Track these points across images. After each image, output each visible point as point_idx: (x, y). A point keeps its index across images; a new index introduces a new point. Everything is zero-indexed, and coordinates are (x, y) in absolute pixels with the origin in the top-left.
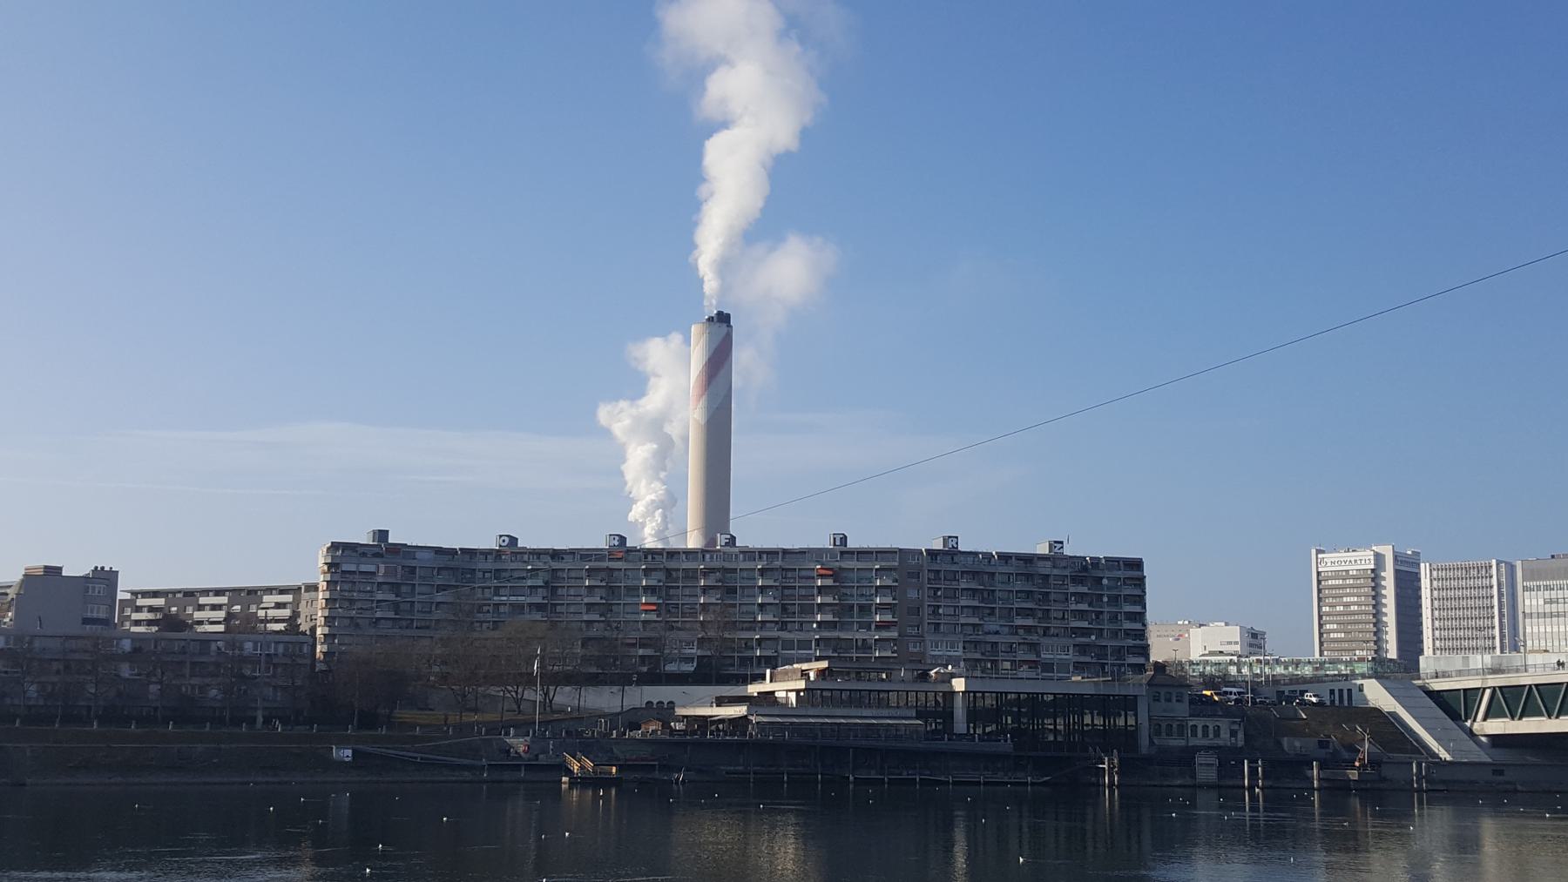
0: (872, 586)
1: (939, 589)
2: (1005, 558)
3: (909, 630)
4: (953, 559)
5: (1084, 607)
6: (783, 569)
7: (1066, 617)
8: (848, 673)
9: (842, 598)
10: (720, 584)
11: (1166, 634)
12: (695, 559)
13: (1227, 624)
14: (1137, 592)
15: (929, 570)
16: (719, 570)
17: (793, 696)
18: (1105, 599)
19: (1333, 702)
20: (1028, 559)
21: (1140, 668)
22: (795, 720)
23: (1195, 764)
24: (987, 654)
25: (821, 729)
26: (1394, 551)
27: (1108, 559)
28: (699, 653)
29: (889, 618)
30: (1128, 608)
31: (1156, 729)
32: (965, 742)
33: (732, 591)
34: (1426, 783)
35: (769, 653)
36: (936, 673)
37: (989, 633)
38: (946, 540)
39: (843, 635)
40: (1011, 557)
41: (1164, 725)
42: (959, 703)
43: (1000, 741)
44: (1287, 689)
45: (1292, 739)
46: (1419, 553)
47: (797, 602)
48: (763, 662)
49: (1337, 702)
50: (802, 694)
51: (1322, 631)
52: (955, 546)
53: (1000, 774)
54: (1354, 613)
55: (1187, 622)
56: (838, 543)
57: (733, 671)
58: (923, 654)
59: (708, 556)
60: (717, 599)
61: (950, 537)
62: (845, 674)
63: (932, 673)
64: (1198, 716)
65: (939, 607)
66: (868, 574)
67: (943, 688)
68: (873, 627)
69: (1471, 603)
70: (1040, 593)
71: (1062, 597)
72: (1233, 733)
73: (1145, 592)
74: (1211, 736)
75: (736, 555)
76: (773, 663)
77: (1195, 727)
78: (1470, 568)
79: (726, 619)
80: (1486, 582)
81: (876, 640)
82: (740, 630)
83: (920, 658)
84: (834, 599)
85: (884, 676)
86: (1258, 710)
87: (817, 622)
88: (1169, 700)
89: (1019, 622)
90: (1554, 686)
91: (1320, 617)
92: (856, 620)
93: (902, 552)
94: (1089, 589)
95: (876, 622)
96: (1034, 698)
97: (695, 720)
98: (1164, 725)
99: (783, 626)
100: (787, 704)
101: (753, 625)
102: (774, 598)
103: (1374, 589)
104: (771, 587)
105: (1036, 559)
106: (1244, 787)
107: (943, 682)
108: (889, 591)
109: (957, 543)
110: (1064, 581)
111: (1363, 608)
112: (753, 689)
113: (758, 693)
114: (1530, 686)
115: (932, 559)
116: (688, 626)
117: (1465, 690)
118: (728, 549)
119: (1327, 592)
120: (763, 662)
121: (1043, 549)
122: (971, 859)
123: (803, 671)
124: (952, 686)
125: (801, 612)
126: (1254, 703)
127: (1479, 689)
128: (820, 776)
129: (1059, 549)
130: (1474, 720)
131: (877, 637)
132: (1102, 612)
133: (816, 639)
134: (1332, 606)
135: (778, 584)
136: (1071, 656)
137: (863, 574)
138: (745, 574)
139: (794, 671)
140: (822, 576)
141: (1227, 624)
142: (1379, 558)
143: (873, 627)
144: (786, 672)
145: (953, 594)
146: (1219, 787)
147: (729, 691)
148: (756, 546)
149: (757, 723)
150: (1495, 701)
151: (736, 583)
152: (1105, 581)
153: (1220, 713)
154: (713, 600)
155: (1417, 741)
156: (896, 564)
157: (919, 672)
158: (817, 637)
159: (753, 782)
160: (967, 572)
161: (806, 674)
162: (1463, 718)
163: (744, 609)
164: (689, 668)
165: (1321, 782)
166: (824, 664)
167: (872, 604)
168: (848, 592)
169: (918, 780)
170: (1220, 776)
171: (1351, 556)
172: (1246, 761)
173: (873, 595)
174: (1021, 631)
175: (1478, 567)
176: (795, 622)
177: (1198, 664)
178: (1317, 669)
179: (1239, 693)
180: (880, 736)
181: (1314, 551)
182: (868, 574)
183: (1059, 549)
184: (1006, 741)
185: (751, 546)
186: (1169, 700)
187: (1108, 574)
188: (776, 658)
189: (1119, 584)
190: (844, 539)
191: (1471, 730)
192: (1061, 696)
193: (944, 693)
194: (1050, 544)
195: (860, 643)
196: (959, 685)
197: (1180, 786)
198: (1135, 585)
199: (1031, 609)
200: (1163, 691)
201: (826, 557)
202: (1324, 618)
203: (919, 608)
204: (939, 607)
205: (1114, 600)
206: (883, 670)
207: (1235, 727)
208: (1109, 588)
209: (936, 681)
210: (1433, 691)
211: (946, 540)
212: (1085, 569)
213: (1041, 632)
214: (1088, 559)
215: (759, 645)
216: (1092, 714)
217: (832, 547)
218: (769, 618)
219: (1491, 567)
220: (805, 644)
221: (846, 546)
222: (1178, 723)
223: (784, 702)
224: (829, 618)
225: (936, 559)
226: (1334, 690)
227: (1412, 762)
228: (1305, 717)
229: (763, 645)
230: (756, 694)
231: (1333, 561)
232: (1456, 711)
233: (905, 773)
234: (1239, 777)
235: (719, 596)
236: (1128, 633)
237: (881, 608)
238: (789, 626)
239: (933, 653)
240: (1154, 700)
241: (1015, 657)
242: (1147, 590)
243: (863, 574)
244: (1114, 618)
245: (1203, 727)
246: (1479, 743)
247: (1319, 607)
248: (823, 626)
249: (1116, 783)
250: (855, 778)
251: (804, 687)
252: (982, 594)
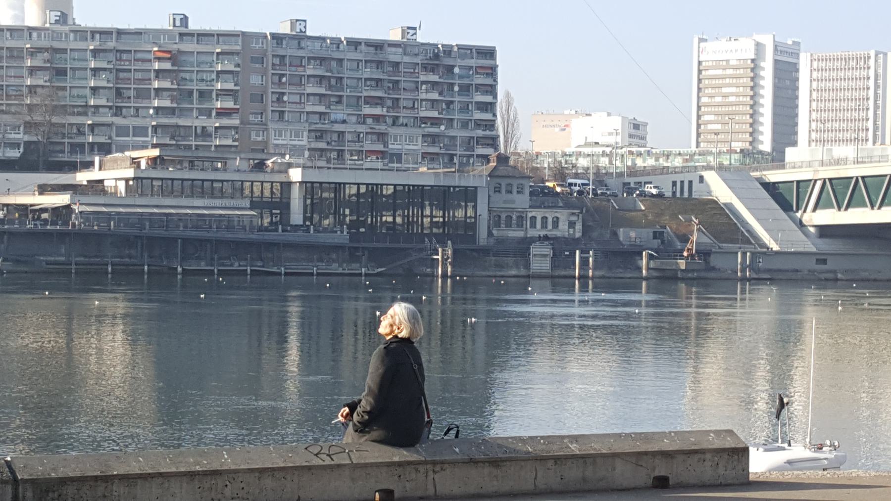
0: (213, 71)
1: (283, 75)
2: (354, 44)
3: (252, 118)
4: (299, 43)
5: (435, 96)
6: (117, 51)
7: (416, 107)
8: (181, 162)
9: (181, 83)
10: (49, 65)
11: (552, 124)
12: (21, 37)
13: (609, 114)
14: (489, 81)
15: (273, 55)
16: (47, 50)
17: (122, 186)
18: (456, 88)
19: (674, 193)
20: (378, 46)
21: (486, 158)
22: (121, 210)
23: (529, 254)
24: (333, 143)
25: (150, 220)
26: (774, 41)
27: (460, 47)
28: (26, 138)
29: (230, 104)
30: (479, 98)
31: (496, 220)
32: (300, 233)
33: (61, 73)
34: (750, 271)
35: (102, 139)
36: (272, 163)
37: (336, 122)
38: (294, 23)
39: (182, 122)
40: (360, 43)
41: (503, 216)
42: (296, 194)
43: (336, 232)
44: (632, 180)
45: (627, 229)
46: (800, 43)
47: (133, 86)
48: (96, 149)
49: (678, 195)
50: (131, 183)
51: (700, 122)
52: (303, 30)
53: (335, 265)
54: (731, 104)
55: (573, 112)
56: (178, 23)
57: (65, 157)
58: (266, 143)
59: (35, 35)
60: (46, 81)
61: (297, 20)
62: (178, 162)
63: (269, 163)
64: (540, 207)
65: (283, 94)
66: (208, 59)
67: (281, 178)
68: (214, 114)
69: (848, 94)
70: (390, 81)
71: (413, 85)
72: (572, 225)
73: (497, 82)
74: (550, 227)
75: (66, 34)
76: (105, 149)
77: (534, 218)
78: (849, 58)
79: (54, 103)
80: (864, 73)
81: (216, 128)
82: (69, 115)
83: (263, 148)
84: (172, 84)
85: (219, 165)
86: (598, 202)
87: (154, 108)
88: (510, 192)
89: (367, 110)
90: (878, 178)
91: (699, 108)
92: (195, 106)
93: (245, 36)
94: (440, 78)
95: (217, 109)
96: (374, 190)
97: (15, 209)
98: (503, 216)
99: (118, 111)
100: (116, 193)
101: (85, 110)
102: (108, 81)
103: (752, 79)
104: (105, 69)
105: (386, 46)
106: (574, 277)
107: (280, 172)
108: (230, 76)
109: (305, 27)
110: (414, 69)
111: (741, 99)
112: (83, 177)
113: (88, 181)
114: (857, 178)
115: (278, 44)
116: (13, 109)
117: (798, 182)
118: (58, 27)
119: (707, 82)
120: (96, 149)
121: (395, 36)
122: (304, 351)
123: (134, 159)
124: (289, 177)
125: (137, 97)
126: (595, 194)
127: (810, 180)
128: (146, 268)
129: (412, 35)
130: (805, 211)
131: (217, 125)
132: (452, 102)
133: (153, 126)
134: (711, 97)
135: (112, 67)
136: (418, 146)
137: (203, 58)
138: (76, 55)
139: (123, 160)
140: (159, 59)
141: (609, 114)
142: (759, 47)
143: (214, 114)
144: (115, 160)
145: (299, 81)
146: (552, 277)
147: (56, 179)
148: (213, 28)
149: (81, 212)
150: (824, 195)
151: (67, 64)
152: (457, 70)
153: (561, 204)
154: (41, 82)
155: (748, 231)
156: (239, 48)
157: (256, 161)
158: (154, 123)
159: (112, 273)
160: (315, 58)
161: (135, 163)
162: (794, 208)
163: (75, 92)
164: (15, 154)
165: (651, 271)
166: (156, 152)
167: (213, 90)
168: (187, 76)
169: (249, 271)
170: (554, 266)
171: (733, 45)
172: (577, 252)
173: (213, 80)
174: (369, 121)
175: (857, 58)
176: (130, 107)
177: (570, 156)
178: (687, 161)
179: (583, 184)
180: (211, 227)
181: (696, 40)
182: (208, 59)
183: (412, 35)
184: (342, 232)
185: (83, 25)
186: (510, 192)
187: (459, 62)
188: (110, 144)
189: (471, 72)
190: (185, 20)
191: (801, 222)
192: (429, 188)
193: (282, 183)
194: (402, 30)
195: (199, 131)
196: (296, 175)
197: (515, 276)
198: (487, 74)
199: (380, 98)
200: (504, 183)
201: (164, 39)
202: (703, 109)
203: (262, 95)
204: (283, 94)
205: (465, 89)
206: (218, 159)
207: (574, 218)
208: (461, 77)
209: (273, 171)
210: (769, 183)
211: (294, 23)
212: (436, 56)
213: (389, 121)
214: (440, 46)
215: (156, 133)
216: (431, 205)
217: (171, 28)
218: (103, 102)
219: (869, 58)
220: (140, 131)
221: (187, 27)
222: (518, 214)
223: (113, 190)
224: (167, 103)
225: (282, 44)
226: (676, 182)
227: (737, 253)
228: (643, 208)
229: (96, 131)
230: (85, 183)
231: (714, 51)
232: (790, 203)
233: (237, 264)
234: (572, 267)
235: (47, 78)
236: (478, 124)
237: (224, 93)
238: (124, 110)
239: (276, 142)
240: (495, 191)
241: (362, 146)
242: (499, 80)
243: (203, 58)
244: (465, 108)
245: (542, 218)
246: (806, 234)
247: (699, 98)
248: (160, 112)
249: (449, 274)
250: (183, 270)
251: (132, 176)
252: (330, 81)
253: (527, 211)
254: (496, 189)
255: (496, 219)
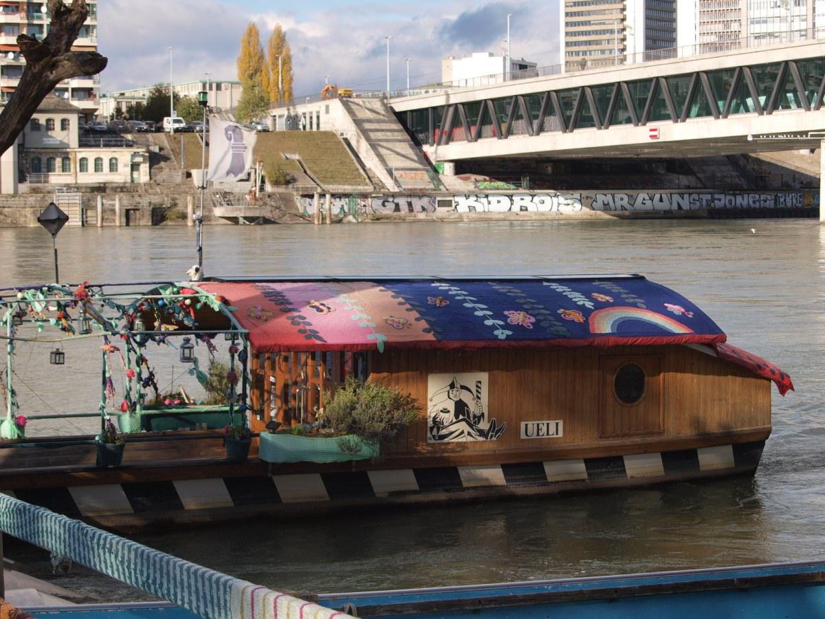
77: (83, 160)
253: (76, 152)
254: (568, 4)
255: (36, 162)
